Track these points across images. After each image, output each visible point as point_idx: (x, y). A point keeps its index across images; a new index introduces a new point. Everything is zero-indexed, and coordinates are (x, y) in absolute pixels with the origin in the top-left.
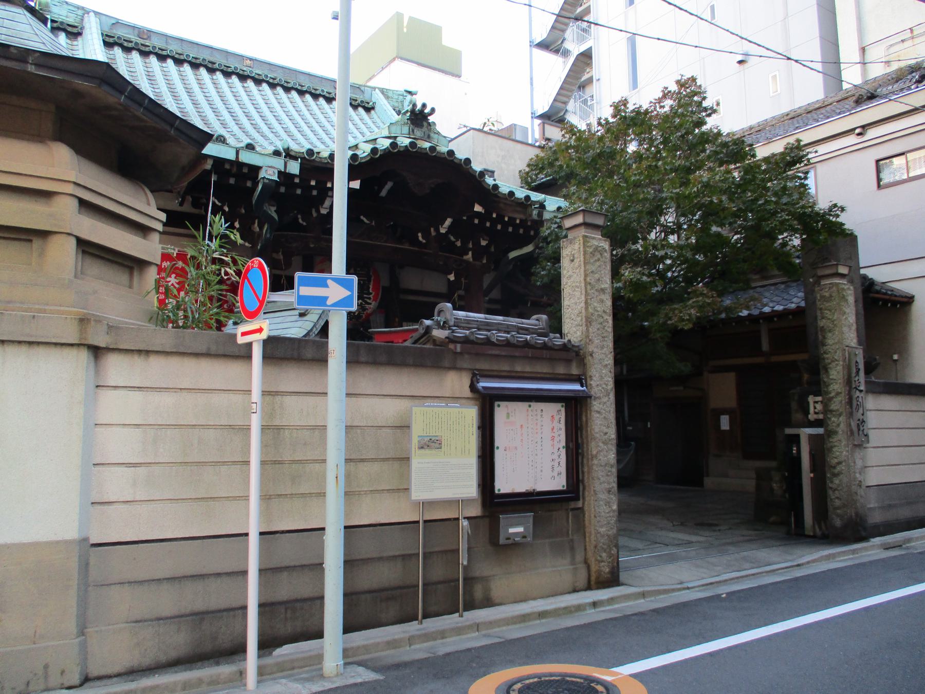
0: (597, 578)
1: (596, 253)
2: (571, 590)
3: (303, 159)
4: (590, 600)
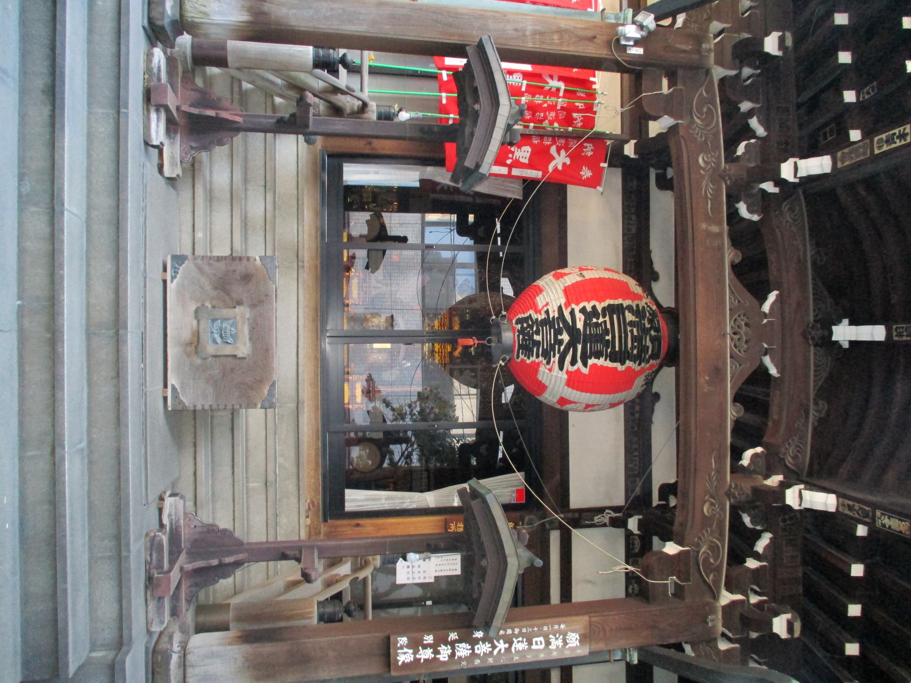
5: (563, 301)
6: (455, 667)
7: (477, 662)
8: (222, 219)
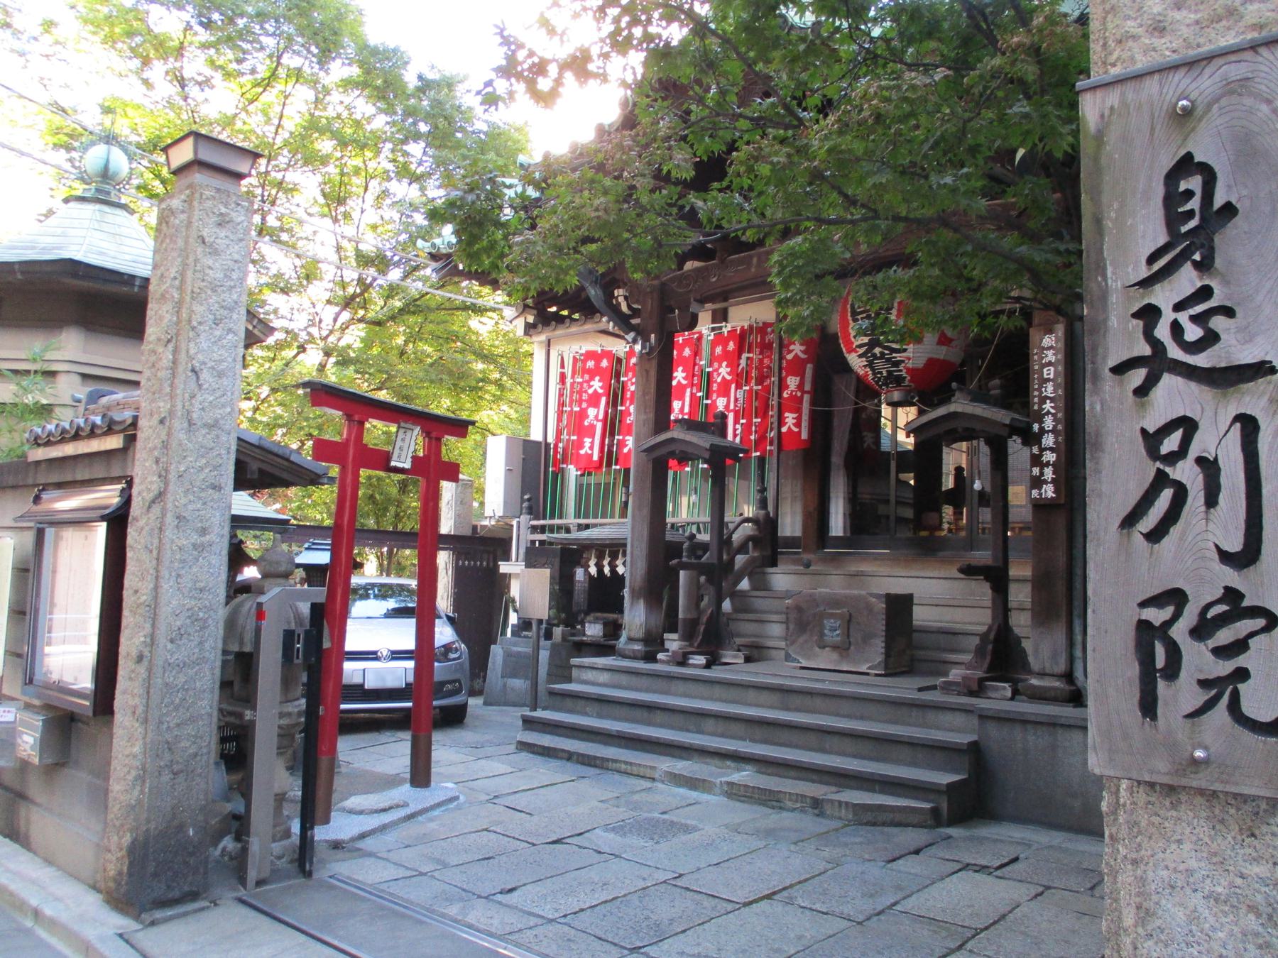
6: (1063, 447)
7: (1060, 427)
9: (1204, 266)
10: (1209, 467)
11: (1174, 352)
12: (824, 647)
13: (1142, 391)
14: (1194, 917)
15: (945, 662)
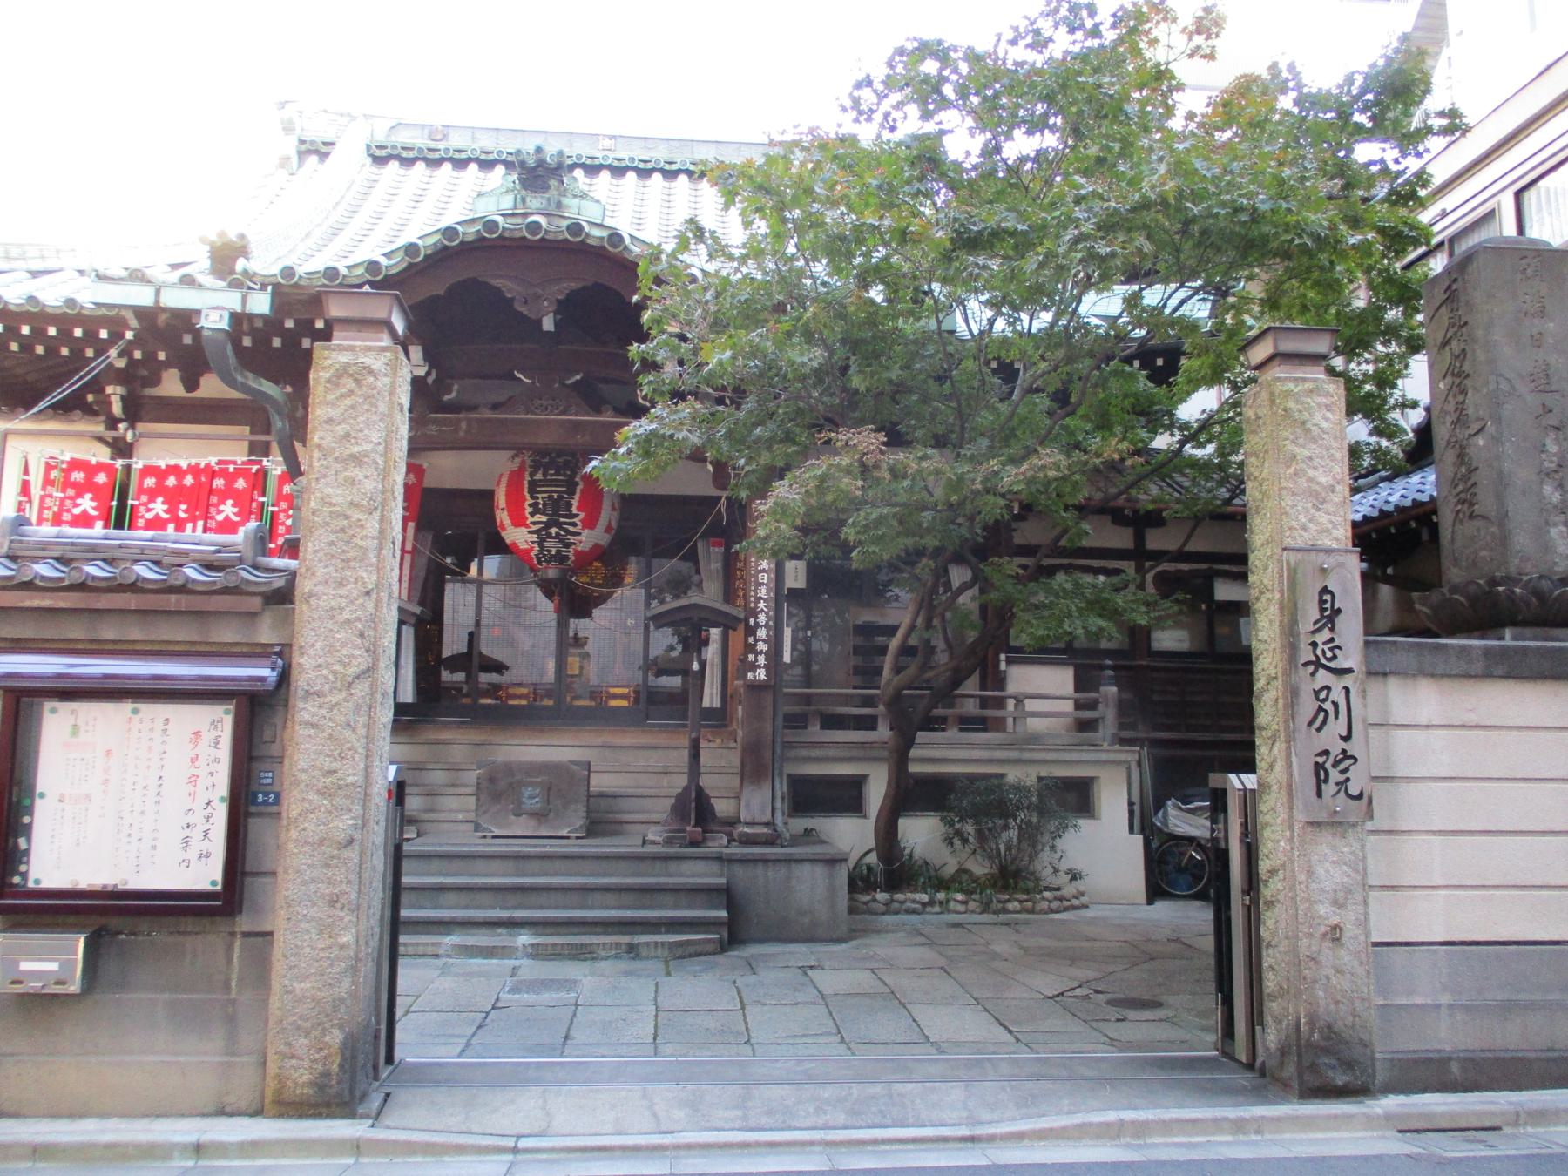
0: (278, 1092)
1: (344, 380)
2: (212, 1109)
3: (276, 286)
4: (192, 1138)
5: (524, 529)
8: (449, 802)
9: (1332, 629)
10: (1335, 704)
11: (1323, 661)
12: (519, 815)
13: (1313, 674)
14: (1327, 871)
15: (621, 823)
